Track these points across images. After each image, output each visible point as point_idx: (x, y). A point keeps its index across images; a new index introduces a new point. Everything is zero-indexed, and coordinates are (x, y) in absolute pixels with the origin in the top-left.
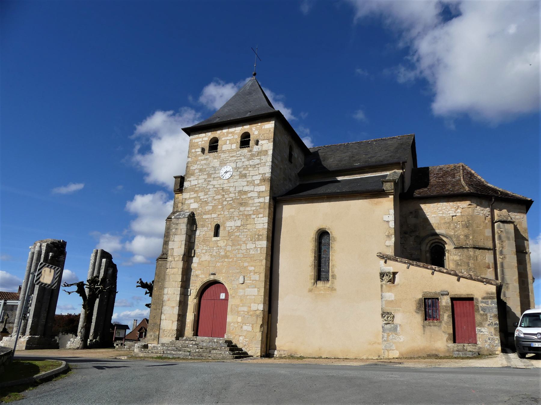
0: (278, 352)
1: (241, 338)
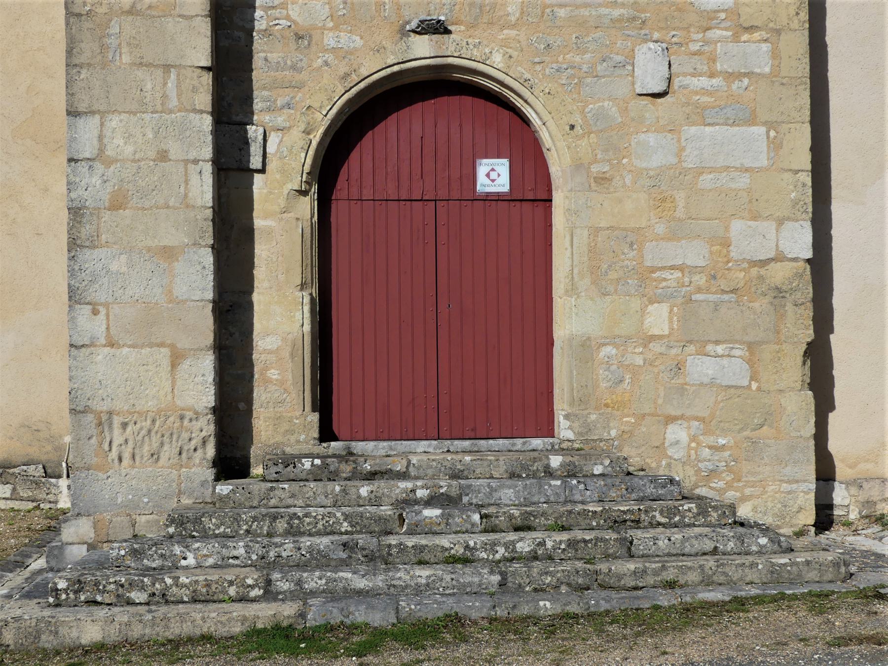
0: (854, 490)
1: (677, 433)
